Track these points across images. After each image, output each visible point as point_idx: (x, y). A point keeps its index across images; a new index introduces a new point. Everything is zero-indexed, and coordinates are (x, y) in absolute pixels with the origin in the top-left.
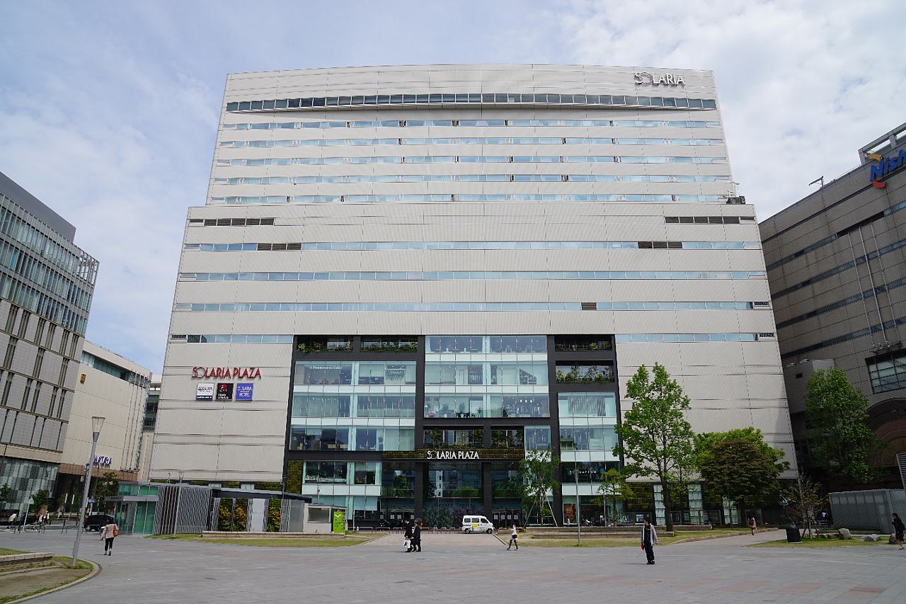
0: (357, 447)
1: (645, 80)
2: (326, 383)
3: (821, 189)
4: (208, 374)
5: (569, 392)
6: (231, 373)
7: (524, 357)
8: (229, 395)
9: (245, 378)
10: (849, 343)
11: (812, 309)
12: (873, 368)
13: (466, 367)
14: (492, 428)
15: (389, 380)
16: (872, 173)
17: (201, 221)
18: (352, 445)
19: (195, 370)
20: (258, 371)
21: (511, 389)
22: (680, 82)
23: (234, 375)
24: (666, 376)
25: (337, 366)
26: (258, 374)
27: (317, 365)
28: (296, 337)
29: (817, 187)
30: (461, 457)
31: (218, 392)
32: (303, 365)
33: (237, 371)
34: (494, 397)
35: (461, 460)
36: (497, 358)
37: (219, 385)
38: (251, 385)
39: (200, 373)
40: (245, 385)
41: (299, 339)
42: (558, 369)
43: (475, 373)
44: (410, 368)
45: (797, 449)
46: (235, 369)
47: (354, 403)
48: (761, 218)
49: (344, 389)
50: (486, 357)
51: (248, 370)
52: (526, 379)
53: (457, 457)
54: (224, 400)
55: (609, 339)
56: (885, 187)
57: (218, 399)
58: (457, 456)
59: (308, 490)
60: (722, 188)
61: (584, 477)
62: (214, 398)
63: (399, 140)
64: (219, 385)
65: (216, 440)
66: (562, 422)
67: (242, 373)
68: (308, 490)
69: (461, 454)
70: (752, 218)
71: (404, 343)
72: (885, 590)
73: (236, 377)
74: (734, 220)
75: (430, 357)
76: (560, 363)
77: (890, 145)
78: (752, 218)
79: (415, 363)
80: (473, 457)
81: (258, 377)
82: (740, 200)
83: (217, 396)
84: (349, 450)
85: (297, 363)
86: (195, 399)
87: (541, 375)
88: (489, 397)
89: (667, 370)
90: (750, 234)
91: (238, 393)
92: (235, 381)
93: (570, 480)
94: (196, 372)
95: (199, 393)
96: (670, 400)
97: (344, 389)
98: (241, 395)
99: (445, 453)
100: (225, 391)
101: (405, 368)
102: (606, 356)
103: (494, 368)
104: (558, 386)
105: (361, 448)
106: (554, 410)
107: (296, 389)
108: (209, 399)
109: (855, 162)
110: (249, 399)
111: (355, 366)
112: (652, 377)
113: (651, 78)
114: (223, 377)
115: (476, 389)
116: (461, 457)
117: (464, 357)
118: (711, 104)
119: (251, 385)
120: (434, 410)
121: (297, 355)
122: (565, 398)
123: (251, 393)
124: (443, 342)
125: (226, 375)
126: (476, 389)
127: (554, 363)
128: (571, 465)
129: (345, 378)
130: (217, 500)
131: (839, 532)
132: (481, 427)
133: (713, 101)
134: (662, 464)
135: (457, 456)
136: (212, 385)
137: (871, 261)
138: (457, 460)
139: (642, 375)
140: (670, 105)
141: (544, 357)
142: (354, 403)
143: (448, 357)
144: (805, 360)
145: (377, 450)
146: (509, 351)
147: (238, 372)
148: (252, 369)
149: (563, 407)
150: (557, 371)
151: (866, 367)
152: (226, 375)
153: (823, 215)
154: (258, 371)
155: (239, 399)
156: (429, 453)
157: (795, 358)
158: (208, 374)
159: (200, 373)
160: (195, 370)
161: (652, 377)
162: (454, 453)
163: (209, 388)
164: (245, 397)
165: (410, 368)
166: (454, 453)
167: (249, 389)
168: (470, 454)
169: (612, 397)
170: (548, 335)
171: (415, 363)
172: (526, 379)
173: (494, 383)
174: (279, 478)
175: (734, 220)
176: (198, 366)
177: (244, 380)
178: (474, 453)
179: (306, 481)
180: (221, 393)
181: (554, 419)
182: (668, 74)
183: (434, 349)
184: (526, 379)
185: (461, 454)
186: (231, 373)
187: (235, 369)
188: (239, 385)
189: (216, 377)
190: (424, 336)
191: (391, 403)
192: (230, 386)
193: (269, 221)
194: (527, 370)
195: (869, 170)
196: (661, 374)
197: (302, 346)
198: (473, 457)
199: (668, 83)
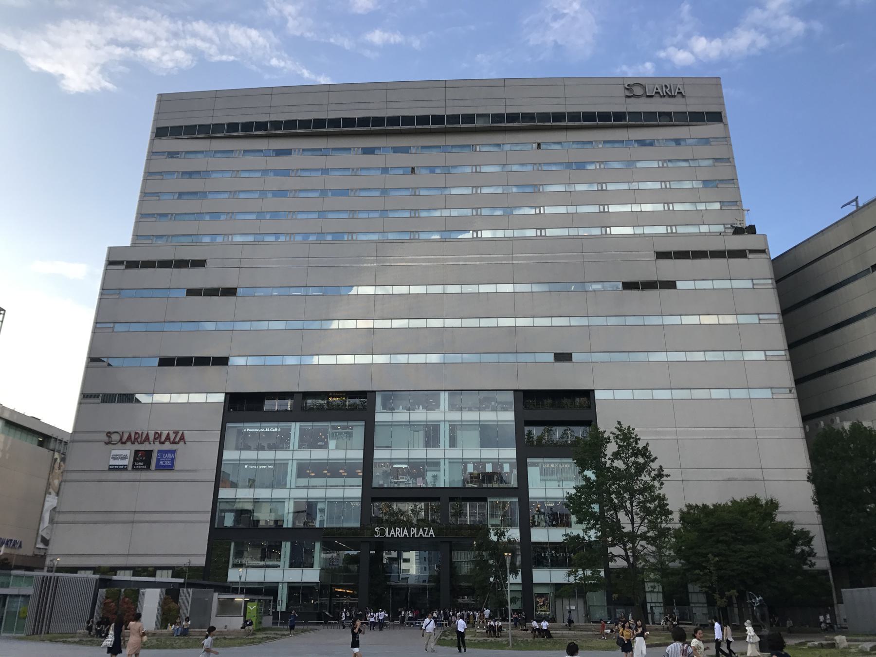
0: (294, 523)
1: (638, 91)
2: (260, 448)
4: (163, 439)
5: (558, 457)
6: (151, 438)
9: (167, 443)
13: (422, 427)
17: (121, 263)
19: (109, 434)
21: (473, 453)
22: (656, 93)
23: (155, 439)
25: (273, 428)
26: (182, 438)
27: (251, 428)
28: (228, 396)
31: (135, 461)
32: (236, 427)
33: (158, 436)
37: (137, 452)
38: (173, 452)
39: (115, 437)
44: (358, 430)
46: (156, 433)
47: (292, 469)
48: (774, 254)
53: (409, 535)
54: (141, 469)
55: (588, 394)
57: (134, 468)
59: (234, 575)
60: (731, 218)
62: (130, 468)
63: (412, 168)
64: (137, 452)
65: (129, 517)
66: (535, 493)
68: (234, 575)
69: (413, 531)
70: (763, 251)
71: (352, 401)
73: (157, 443)
74: (741, 254)
75: (381, 416)
78: (763, 251)
79: (363, 423)
81: (182, 443)
82: (751, 230)
83: (133, 465)
84: (285, 526)
85: (229, 425)
86: (107, 469)
88: (447, 461)
90: (761, 267)
91: (158, 461)
92: (156, 447)
93: (541, 563)
94: (109, 437)
96: (640, 469)
98: (161, 463)
100: (143, 460)
101: (352, 429)
102: (583, 416)
103: (454, 427)
105: (237, 526)
106: (523, 477)
107: (227, 455)
108: (124, 468)
110: (171, 468)
113: (644, 87)
114: (142, 443)
116: (413, 535)
117: (419, 416)
118: (716, 117)
119: (173, 452)
122: (534, 465)
123: (173, 460)
125: (145, 440)
126: (433, 454)
127: (522, 422)
129: (282, 443)
130: (102, 592)
133: (720, 113)
135: (409, 535)
136: (127, 453)
140: (666, 118)
141: (509, 416)
145: (318, 526)
147: (160, 435)
148: (176, 433)
149: (534, 473)
150: (526, 432)
151: (224, 391)
152: (145, 440)
154: (183, 433)
155: (159, 468)
156: (377, 529)
158: (125, 438)
159: (115, 437)
162: (405, 530)
163: (125, 454)
165: (358, 430)
166: (405, 530)
167: (170, 456)
170: (515, 391)
171: (363, 423)
173: (453, 444)
175: (741, 254)
176: (112, 430)
177: (167, 446)
178: (429, 531)
182: (678, 86)
183: (386, 407)
185: (413, 531)
186: (151, 438)
187: (156, 433)
188: (159, 451)
189: (133, 443)
190: (375, 392)
191: (331, 470)
192: (149, 453)
199: (665, 94)
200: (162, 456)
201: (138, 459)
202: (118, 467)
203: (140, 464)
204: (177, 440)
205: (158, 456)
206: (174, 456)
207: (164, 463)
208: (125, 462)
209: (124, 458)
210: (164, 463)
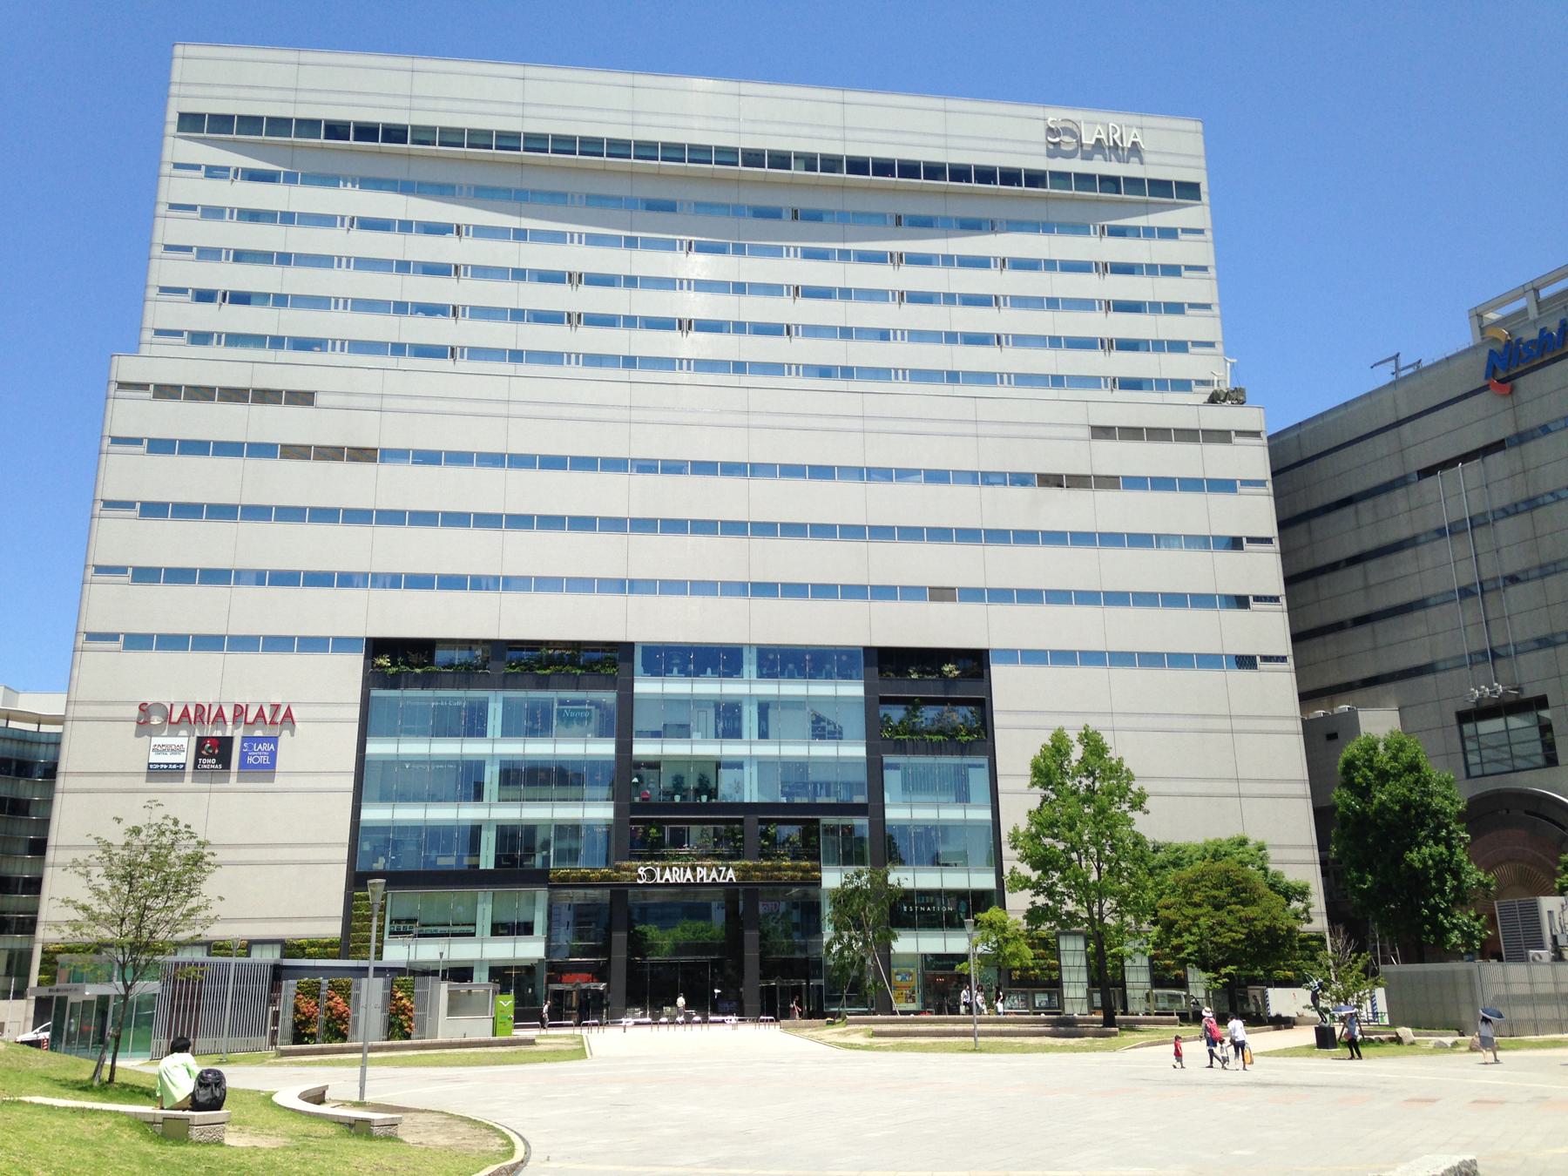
3: (1392, 384)
6: (228, 713)
7: (821, 689)
8: (225, 761)
10: (1428, 679)
11: (1361, 610)
12: (1468, 728)
14: (761, 822)
15: (562, 728)
16: (1488, 366)
18: (388, 991)
19: (144, 708)
20: (289, 708)
21: (795, 750)
24: (1104, 750)
26: (289, 714)
29: (1384, 376)
30: (702, 879)
33: (240, 711)
34: (763, 763)
35: (702, 885)
36: (768, 689)
38: (274, 740)
40: (260, 740)
41: (376, 647)
42: (884, 710)
43: (728, 719)
45: (1324, 874)
47: (491, 777)
49: (473, 748)
50: (747, 687)
51: (264, 709)
52: (822, 729)
56: (1511, 393)
58: (695, 877)
61: (932, 918)
62: (190, 767)
64: (201, 741)
66: (893, 814)
67: (251, 717)
72: (1438, 1100)
75: (645, 686)
76: (885, 701)
77: (1524, 311)
80: (724, 878)
83: (196, 763)
87: (855, 722)
89: (1107, 738)
91: (243, 756)
95: (154, 758)
97: (473, 748)
98: (250, 760)
99: (671, 870)
100: (214, 753)
103: (764, 708)
104: (883, 740)
108: (175, 772)
109: (1463, 337)
111: (496, 704)
112: (1077, 753)
115: (732, 749)
116: (702, 879)
117: (709, 687)
120: (655, 789)
121: (374, 678)
122: (895, 767)
123: (273, 755)
124: (667, 658)
126: (732, 749)
127: (875, 702)
128: (909, 895)
129: (474, 725)
131: (1397, 1034)
132: (740, 821)
134: (1096, 909)
135: (695, 877)
137: (1476, 531)
138: (695, 885)
139: (1058, 748)
142: (491, 777)
143: (677, 687)
144: (1345, 707)
146: (791, 676)
149: (892, 779)
153: (1391, 434)
157: (1325, 700)
158: (176, 716)
160: (144, 708)
161: (1077, 753)
163: (179, 747)
164: (261, 766)
168: (719, 872)
169: (981, 766)
172: (824, 728)
173: (763, 735)
174: (334, 930)
179: (392, 933)
180: (204, 757)
181: (874, 808)
184: (824, 728)
186: (228, 713)
187: (236, 706)
193: (304, 398)
194: (825, 713)
195: (1484, 354)
196: (1094, 746)
197: (384, 661)
198: (724, 878)
200: (251, 747)
201: (204, 752)
202: (166, 767)
203: (209, 761)
204: (279, 719)
205: (242, 747)
206: (276, 747)
207: (256, 760)
208: (180, 758)
209: (177, 750)
210: (256, 760)
